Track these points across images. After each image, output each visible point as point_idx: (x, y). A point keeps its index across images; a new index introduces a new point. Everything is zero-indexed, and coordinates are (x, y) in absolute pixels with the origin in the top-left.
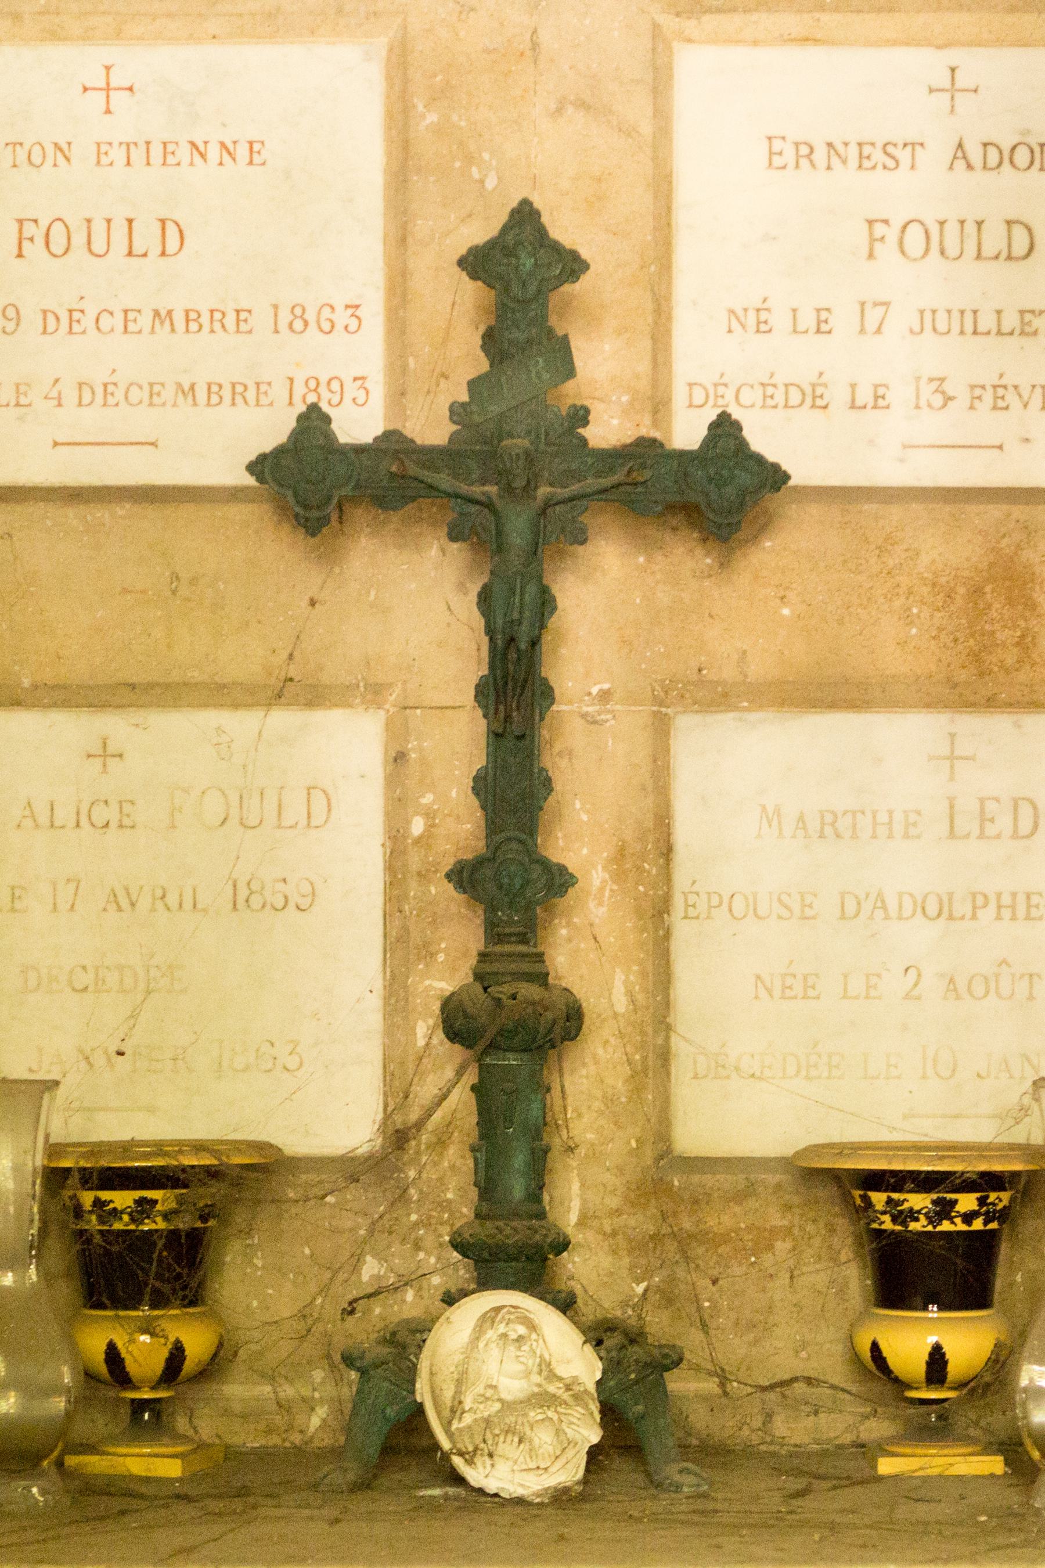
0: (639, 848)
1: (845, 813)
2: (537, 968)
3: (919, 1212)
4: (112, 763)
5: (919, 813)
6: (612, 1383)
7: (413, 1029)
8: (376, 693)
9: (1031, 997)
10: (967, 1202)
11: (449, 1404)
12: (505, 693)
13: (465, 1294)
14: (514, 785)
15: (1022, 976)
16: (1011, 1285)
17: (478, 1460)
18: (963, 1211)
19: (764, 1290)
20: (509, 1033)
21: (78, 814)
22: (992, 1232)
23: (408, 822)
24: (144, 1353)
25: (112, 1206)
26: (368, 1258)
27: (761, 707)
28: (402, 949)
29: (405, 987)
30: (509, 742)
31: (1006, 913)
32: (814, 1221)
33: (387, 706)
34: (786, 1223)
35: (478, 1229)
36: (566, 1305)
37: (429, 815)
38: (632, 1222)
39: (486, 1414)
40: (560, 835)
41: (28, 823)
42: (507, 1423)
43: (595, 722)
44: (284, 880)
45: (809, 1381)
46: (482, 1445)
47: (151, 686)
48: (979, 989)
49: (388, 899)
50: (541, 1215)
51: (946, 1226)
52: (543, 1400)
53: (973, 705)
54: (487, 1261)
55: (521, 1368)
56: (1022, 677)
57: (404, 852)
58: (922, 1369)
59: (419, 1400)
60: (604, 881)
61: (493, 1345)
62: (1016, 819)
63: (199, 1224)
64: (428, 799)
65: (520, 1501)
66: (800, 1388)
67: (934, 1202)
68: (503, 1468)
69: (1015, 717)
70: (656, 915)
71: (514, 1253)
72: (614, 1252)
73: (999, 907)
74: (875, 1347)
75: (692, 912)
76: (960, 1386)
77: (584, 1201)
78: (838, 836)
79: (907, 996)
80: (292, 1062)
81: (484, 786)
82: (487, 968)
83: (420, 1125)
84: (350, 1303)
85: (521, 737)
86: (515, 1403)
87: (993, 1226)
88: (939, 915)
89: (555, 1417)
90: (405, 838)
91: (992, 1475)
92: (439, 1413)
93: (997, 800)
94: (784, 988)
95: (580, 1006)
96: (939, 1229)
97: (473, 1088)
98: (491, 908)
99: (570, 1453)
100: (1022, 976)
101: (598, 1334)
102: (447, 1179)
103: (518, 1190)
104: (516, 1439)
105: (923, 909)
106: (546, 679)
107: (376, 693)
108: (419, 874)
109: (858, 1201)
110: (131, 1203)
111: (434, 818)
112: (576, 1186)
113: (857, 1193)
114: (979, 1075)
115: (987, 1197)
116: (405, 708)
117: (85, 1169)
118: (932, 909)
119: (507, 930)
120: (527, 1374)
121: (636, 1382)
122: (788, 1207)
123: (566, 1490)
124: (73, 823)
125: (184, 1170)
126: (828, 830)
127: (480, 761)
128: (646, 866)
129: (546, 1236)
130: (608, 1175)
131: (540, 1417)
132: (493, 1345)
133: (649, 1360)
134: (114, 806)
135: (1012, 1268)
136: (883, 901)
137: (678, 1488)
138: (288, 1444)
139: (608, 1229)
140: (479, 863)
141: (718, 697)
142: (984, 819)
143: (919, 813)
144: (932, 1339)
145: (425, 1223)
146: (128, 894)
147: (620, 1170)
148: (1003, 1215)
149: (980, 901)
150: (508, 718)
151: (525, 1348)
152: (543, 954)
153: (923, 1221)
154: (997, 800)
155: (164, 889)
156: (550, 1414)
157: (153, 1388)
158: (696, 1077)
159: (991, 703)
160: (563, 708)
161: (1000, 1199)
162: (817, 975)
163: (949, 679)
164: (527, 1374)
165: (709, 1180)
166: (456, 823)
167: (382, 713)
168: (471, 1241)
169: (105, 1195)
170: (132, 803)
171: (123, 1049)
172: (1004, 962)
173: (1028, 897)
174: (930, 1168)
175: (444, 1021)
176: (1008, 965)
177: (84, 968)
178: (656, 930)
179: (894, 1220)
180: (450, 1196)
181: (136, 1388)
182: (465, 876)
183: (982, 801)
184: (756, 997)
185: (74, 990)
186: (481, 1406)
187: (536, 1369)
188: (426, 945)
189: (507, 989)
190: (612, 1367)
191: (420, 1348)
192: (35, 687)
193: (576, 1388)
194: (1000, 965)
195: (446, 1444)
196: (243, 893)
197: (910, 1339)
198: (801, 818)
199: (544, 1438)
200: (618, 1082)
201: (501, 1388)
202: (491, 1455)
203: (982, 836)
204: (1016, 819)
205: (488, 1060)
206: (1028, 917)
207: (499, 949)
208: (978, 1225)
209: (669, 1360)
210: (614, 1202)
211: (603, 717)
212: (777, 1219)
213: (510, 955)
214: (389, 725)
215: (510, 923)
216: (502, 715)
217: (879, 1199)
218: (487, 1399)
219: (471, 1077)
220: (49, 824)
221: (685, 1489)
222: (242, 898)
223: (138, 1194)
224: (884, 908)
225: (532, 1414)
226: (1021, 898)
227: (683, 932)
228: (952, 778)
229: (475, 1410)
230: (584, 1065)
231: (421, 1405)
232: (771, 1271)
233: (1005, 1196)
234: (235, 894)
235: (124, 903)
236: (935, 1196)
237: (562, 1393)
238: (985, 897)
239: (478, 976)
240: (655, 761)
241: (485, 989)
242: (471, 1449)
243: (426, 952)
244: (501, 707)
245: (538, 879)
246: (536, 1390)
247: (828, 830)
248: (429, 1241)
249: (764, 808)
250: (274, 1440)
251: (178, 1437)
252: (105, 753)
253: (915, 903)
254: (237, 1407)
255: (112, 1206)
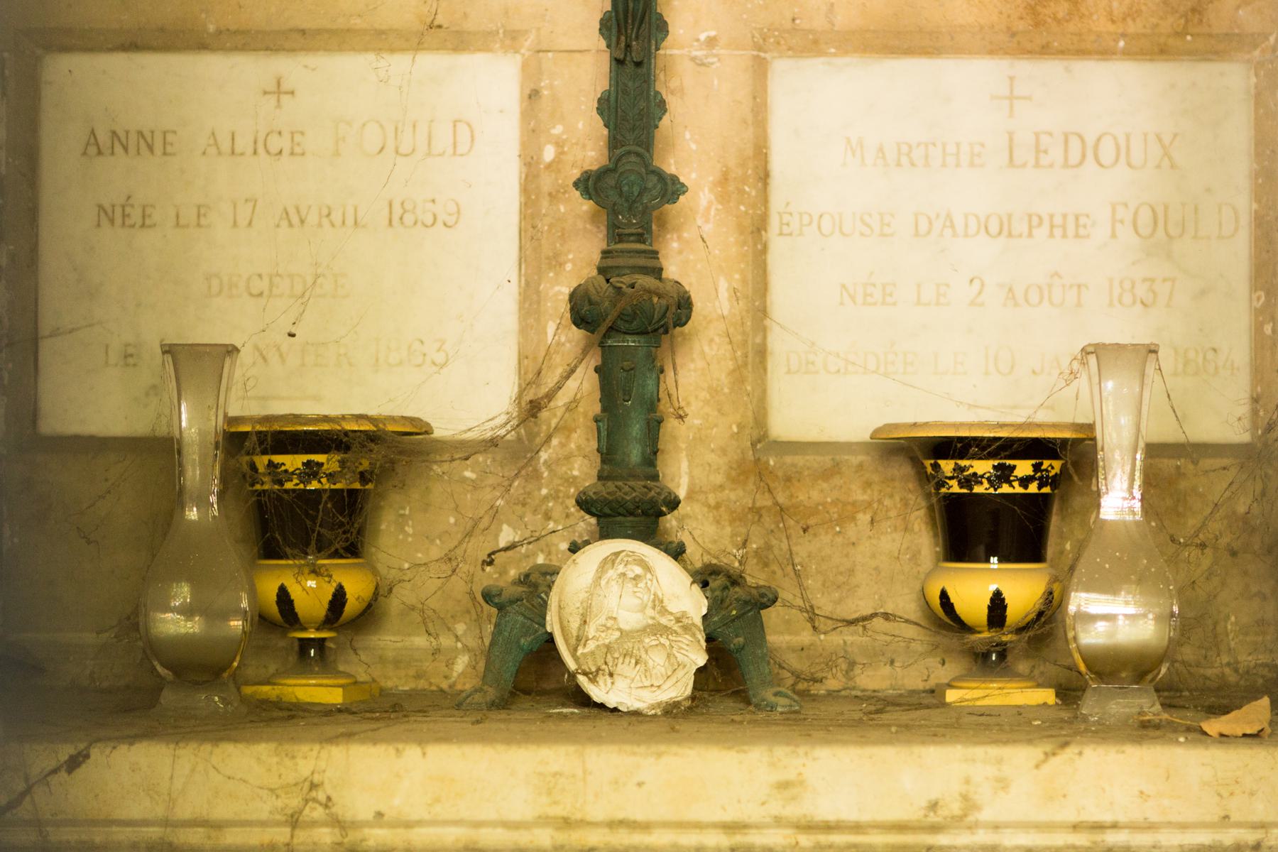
0: (740, 173)
1: (919, 144)
2: (650, 263)
3: (982, 477)
4: (285, 98)
5: (983, 145)
6: (716, 619)
7: (545, 328)
8: (514, 39)
9: (1079, 305)
10: (1024, 468)
11: (575, 634)
12: (626, 22)
13: (587, 543)
14: (632, 106)
15: (1071, 286)
16: (1062, 552)
17: (600, 679)
18: (1020, 475)
19: (847, 556)
20: (629, 322)
21: (255, 142)
22: (1047, 495)
23: (540, 149)
24: (311, 594)
25: (283, 468)
26: (505, 527)
27: (846, 53)
28: (535, 254)
29: (538, 292)
30: (630, 68)
31: (1058, 232)
32: (891, 496)
33: (523, 51)
34: (866, 497)
35: (600, 487)
36: (677, 553)
37: (559, 144)
38: (733, 496)
39: (607, 641)
40: (672, 161)
41: (212, 150)
42: (626, 647)
43: (703, 64)
44: (433, 201)
45: (886, 616)
46: (604, 667)
47: (319, 32)
48: (1034, 297)
49: (523, 216)
50: (655, 477)
51: (1005, 489)
52: (657, 629)
53: (1030, 52)
54: (609, 516)
55: (637, 601)
56: (1071, 27)
57: (537, 176)
58: (984, 613)
59: (549, 629)
60: (710, 203)
61: (613, 583)
62: (1066, 151)
63: (357, 486)
64: (558, 130)
65: (636, 713)
66: (878, 623)
67: (994, 467)
68: (621, 683)
69: (1066, 63)
70: (756, 230)
71: (629, 508)
72: (718, 522)
73: (1052, 226)
74: (944, 595)
75: (786, 230)
76: (1020, 630)
77: (692, 477)
78: (912, 164)
79: (972, 303)
80: (440, 358)
81: (609, 108)
82: (610, 262)
83: (550, 396)
84: (489, 555)
85: (638, 64)
86: (631, 632)
87: (1046, 490)
88: (1000, 233)
89: (667, 643)
90: (538, 163)
91: (1045, 704)
92: (566, 640)
93: (1050, 134)
94: (866, 295)
95: (689, 297)
96: (999, 491)
97: (597, 370)
98: (613, 212)
99: (680, 673)
100: (1071, 286)
101: (704, 578)
102: (573, 459)
103: (635, 454)
104: (633, 661)
105: (986, 228)
106: (661, 15)
107: (514, 39)
108: (550, 194)
109: (929, 470)
110: (300, 466)
111: (562, 147)
112: (684, 465)
113: (928, 463)
114: (1034, 372)
115: (1041, 464)
116: (539, 51)
117: (260, 432)
118: (994, 228)
119: (627, 231)
120: (642, 609)
121: (737, 617)
122: (868, 485)
123: (676, 705)
124: (250, 150)
125: (346, 433)
126: (904, 160)
127: (603, 84)
128: (747, 189)
129: (659, 494)
130: (713, 456)
131: (654, 643)
132: (613, 583)
133: (748, 598)
134: (287, 136)
135: (1062, 537)
136: (951, 221)
137: (772, 708)
138: (434, 688)
139: (712, 501)
140: (602, 173)
141: (811, 44)
142: (1039, 150)
143: (983, 145)
144: (993, 588)
145: (555, 496)
146: (298, 212)
147: (724, 451)
148: (1055, 482)
149: (1035, 221)
150: (628, 46)
151: (642, 585)
152: (657, 253)
153: (986, 484)
154: (1050, 134)
155: (329, 208)
156: (663, 640)
157: (318, 629)
158: (789, 372)
159: (1045, 51)
160: (675, 52)
161: (1053, 466)
162: (894, 285)
163: (1009, 28)
164: (642, 609)
165: (800, 460)
166: (583, 140)
167: (518, 57)
168: (594, 497)
169: (277, 459)
170: (302, 133)
171: (293, 331)
172: (1056, 274)
173: (1077, 219)
174: (992, 435)
175: (572, 309)
176: (1060, 277)
177: (260, 276)
178: (755, 245)
179: (961, 485)
180: (576, 473)
181: (304, 629)
182: (590, 184)
183: (1037, 135)
184: (842, 304)
185: (251, 295)
186: (603, 635)
187: (650, 604)
188: (556, 256)
189: (627, 279)
190: (716, 605)
191: (550, 587)
192: (219, 32)
193: (685, 621)
194: (1052, 276)
195: (571, 665)
196: (397, 211)
197: (973, 587)
198: (881, 150)
199: (657, 660)
200: (721, 374)
201: (620, 619)
202: (611, 675)
203: (1037, 165)
204: (1066, 151)
205: (610, 342)
206: (1077, 236)
207: (620, 246)
208: (1033, 488)
209: (765, 599)
210: (719, 479)
211: (710, 60)
212: (860, 496)
213: (629, 252)
214: (525, 66)
215: (630, 225)
216: (623, 45)
217: (947, 466)
218: (608, 628)
219: (594, 360)
220: (229, 151)
221: (780, 709)
222: (397, 216)
223: (305, 458)
224: (952, 226)
225: (647, 640)
226: (1071, 220)
227: (779, 249)
228: (1011, 115)
229: (596, 636)
230: (693, 360)
231: (550, 639)
232: (853, 539)
233: (1057, 465)
234: (391, 213)
235: (295, 220)
236: (996, 463)
237: (672, 624)
238: (1040, 218)
239: (602, 270)
240: (755, 98)
241: (608, 281)
242: (594, 669)
243: (556, 262)
244: (623, 38)
245: (654, 188)
246: (651, 622)
247: (904, 160)
248: (558, 512)
249: (848, 140)
250: (422, 684)
251: (339, 674)
252: (279, 90)
253: (979, 221)
254: (390, 654)
255: (283, 468)
